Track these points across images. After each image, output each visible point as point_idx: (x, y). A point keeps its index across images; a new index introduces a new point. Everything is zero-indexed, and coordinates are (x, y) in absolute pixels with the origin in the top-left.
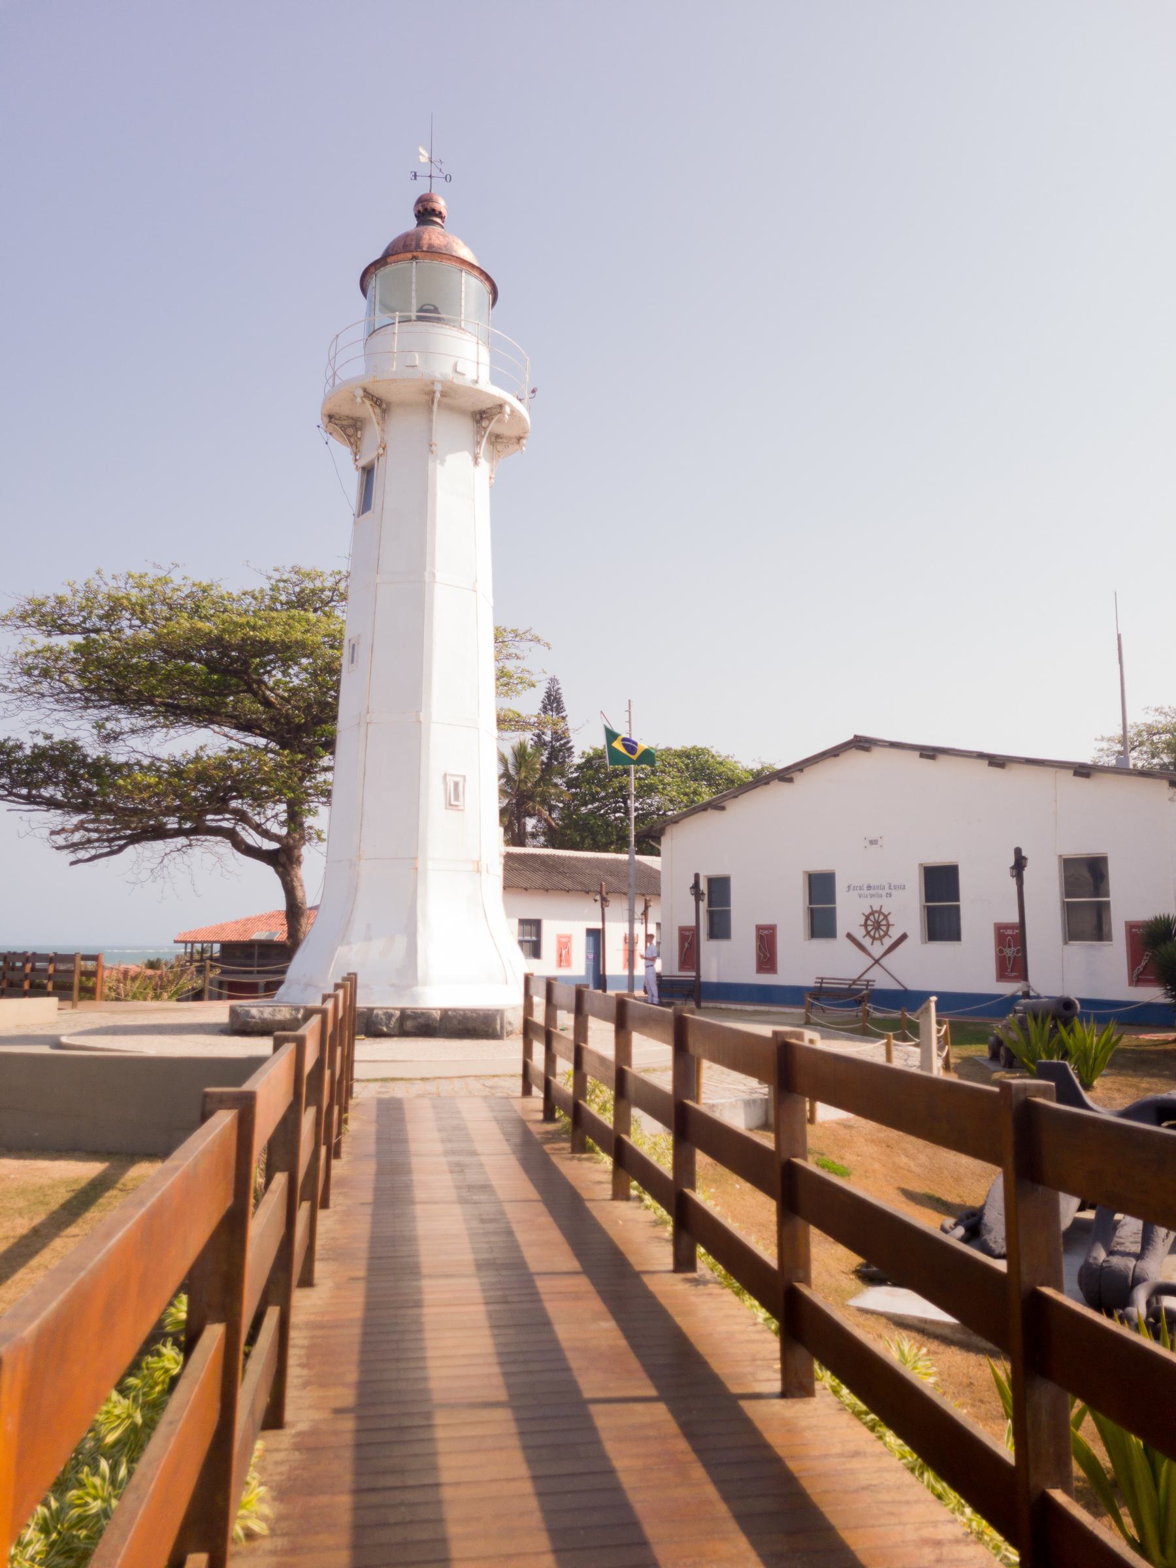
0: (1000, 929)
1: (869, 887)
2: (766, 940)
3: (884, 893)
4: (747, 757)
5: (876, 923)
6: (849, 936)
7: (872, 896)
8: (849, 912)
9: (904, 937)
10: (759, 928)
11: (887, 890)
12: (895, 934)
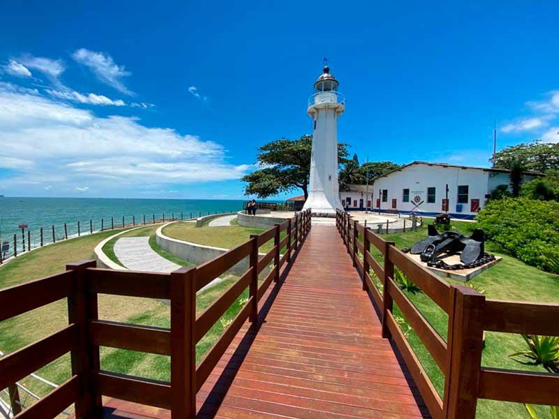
0: (443, 200)
2: (394, 202)
4: (400, 164)
5: (417, 199)
8: (412, 197)
10: (386, 201)
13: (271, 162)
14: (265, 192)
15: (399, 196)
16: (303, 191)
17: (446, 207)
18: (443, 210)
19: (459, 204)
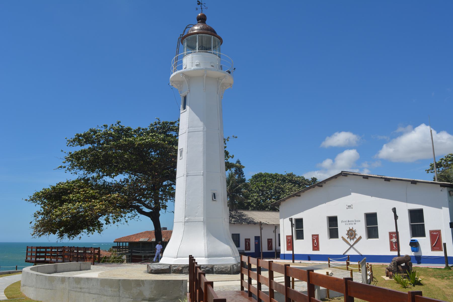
0: (391, 234)
1: (348, 221)
3: (353, 223)
5: (351, 234)
6: (342, 237)
7: (350, 224)
8: (342, 230)
9: (360, 238)
10: (376, 236)
11: (354, 222)
12: (357, 237)
13: (91, 169)
14: (73, 226)
15: (323, 231)
16: (151, 223)
17: (395, 246)
18: (392, 249)
19: (414, 238)
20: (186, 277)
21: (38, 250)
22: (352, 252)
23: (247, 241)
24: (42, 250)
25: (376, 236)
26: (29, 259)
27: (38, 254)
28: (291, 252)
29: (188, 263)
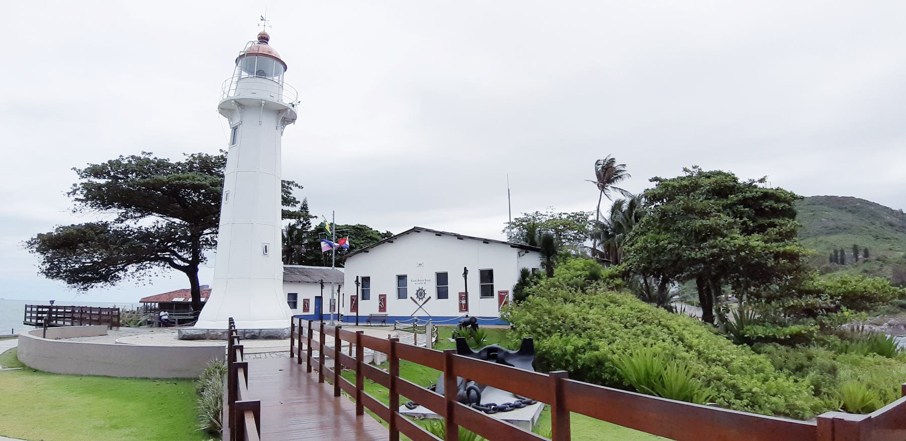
5: (421, 293)
8: (411, 291)
10: (482, 272)
12: (427, 297)
20: (226, 344)
21: (40, 310)
22: (420, 313)
23: (306, 303)
24: (45, 310)
25: (482, 272)
26: (28, 320)
27: (40, 315)
28: (355, 314)
29: (227, 327)
